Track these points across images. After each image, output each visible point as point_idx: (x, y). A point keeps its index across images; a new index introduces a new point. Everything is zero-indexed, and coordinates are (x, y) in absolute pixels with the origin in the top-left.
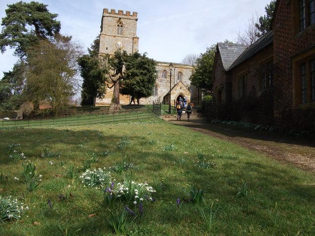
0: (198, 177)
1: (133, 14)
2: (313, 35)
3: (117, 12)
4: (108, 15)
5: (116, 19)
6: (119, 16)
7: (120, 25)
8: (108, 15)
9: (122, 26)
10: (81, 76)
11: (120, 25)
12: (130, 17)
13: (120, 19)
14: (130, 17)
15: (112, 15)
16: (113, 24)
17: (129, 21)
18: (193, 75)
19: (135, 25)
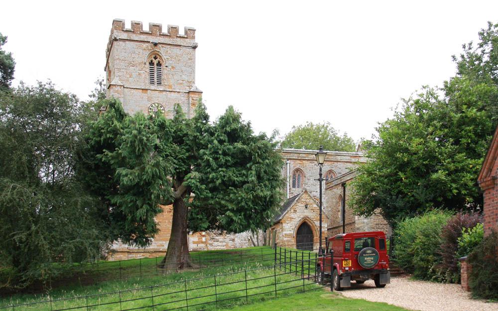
0: (388, 243)
1: (186, 33)
2: (496, 215)
3: (146, 28)
4: (124, 36)
5: (145, 45)
6: (152, 39)
7: (156, 62)
8: (124, 36)
9: (159, 64)
10: (124, 243)
11: (156, 62)
12: (179, 41)
13: (156, 45)
14: (179, 41)
15: (134, 37)
16: (140, 60)
17: (176, 50)
18: (399, 124)
19: (192, 59)
